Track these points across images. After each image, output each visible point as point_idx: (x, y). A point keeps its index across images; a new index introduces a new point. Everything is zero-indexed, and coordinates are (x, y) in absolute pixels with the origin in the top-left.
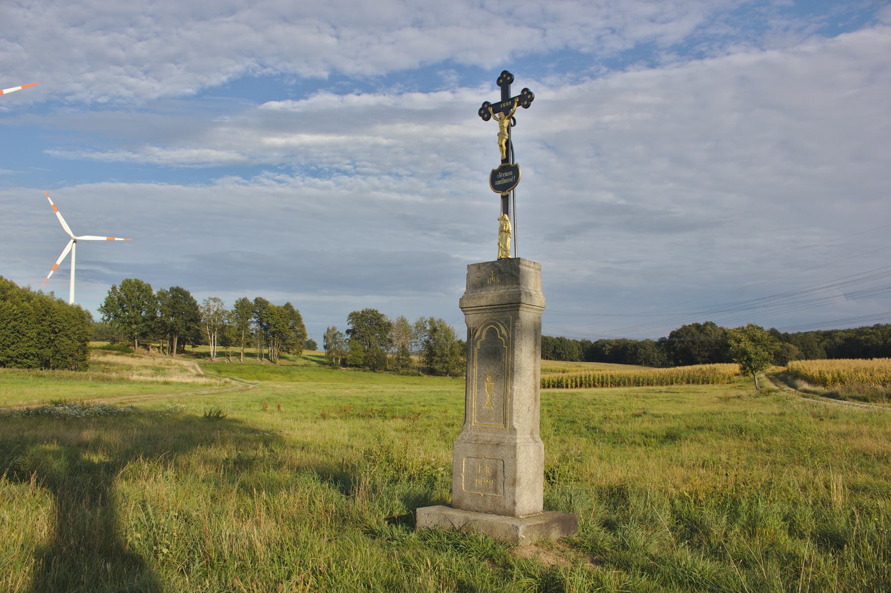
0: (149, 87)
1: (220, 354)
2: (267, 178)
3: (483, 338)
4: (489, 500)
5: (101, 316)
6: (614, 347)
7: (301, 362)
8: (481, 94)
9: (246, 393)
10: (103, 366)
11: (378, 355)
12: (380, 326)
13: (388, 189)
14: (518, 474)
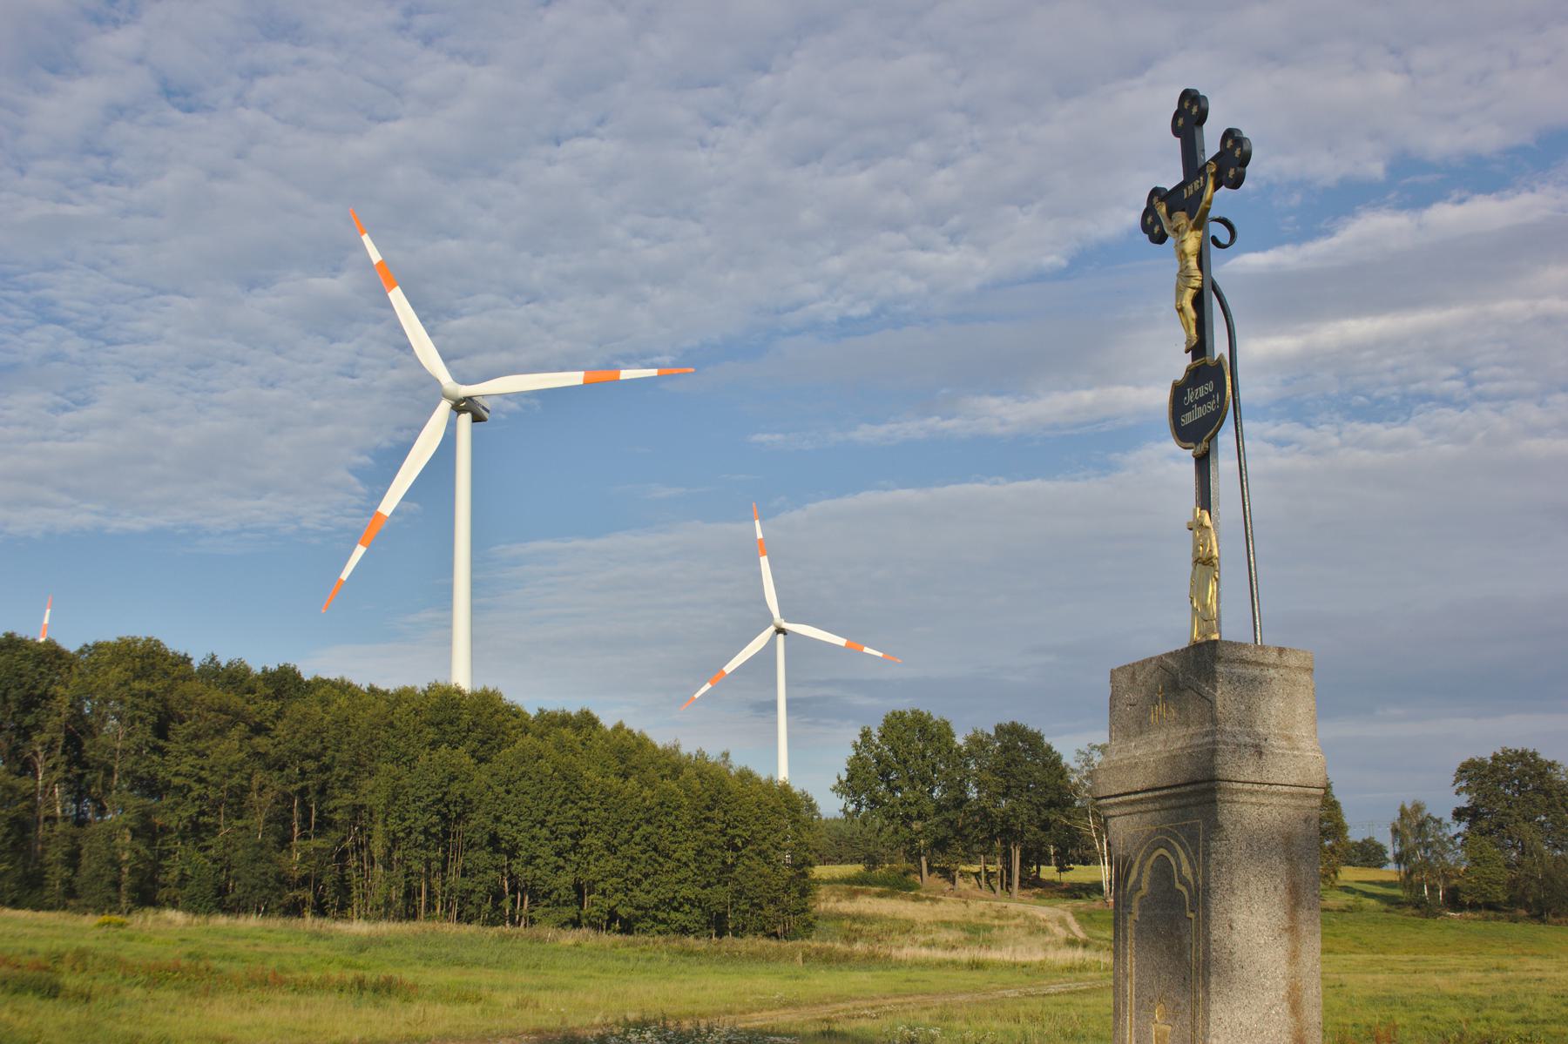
0: (957, 264)
3: (1145, 885)
10: (846, 923)
11: (1547, 875)
12: (1548, 794)
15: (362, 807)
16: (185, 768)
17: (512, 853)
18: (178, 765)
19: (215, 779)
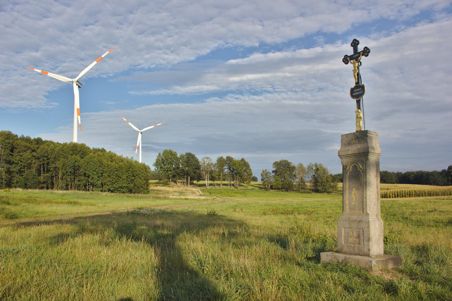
0: (173, 58)
1: (211, 185)
2: (231, 97)
3: (351, 170)
4: (356, 249)
5: (154, 168)
6: (416, 175)
7: (250, 187)
8: (337, 47)
9: (225, 203)
10: (156, 191)
12: (289, 168)
13: (291, 99)
14: (371, 236)
15: (56, 167)
16: (17, 159)
17: (88, 177)
18: (16, 158)
19: (25, 161)
